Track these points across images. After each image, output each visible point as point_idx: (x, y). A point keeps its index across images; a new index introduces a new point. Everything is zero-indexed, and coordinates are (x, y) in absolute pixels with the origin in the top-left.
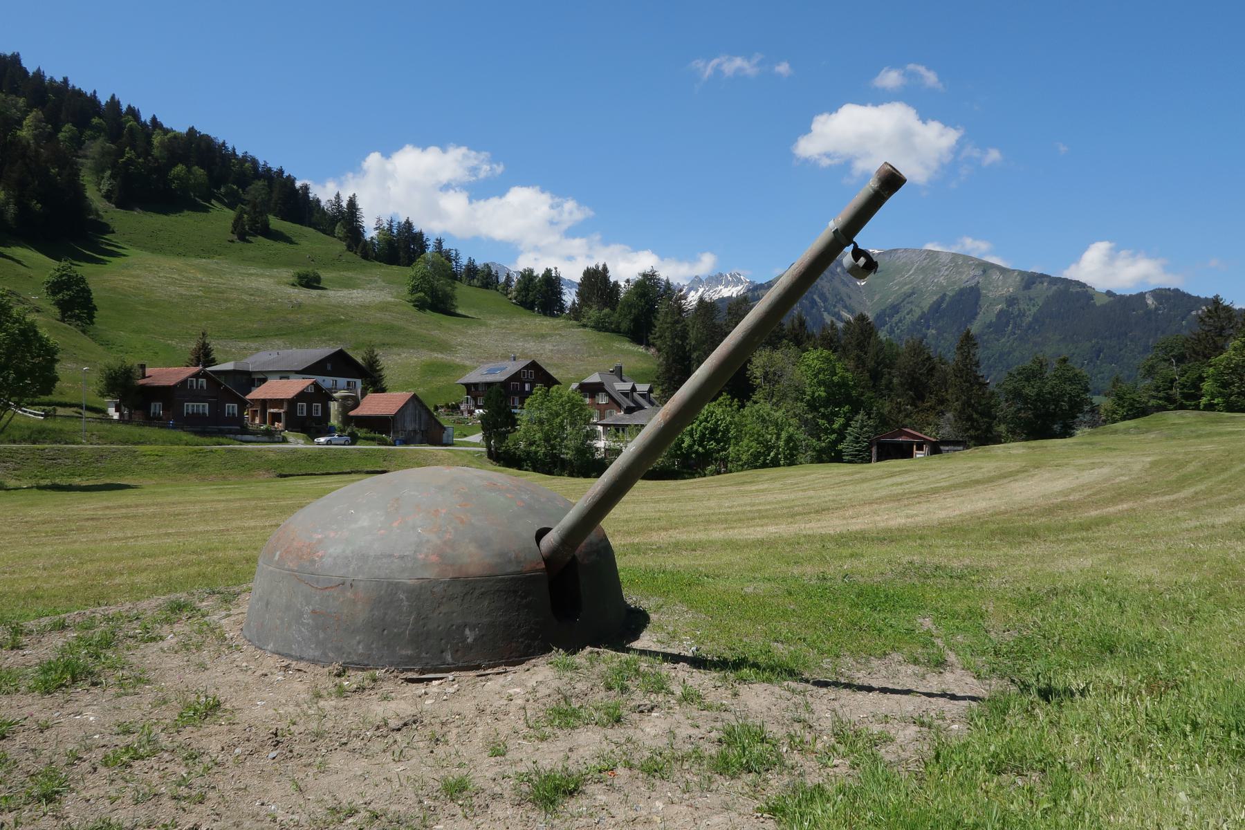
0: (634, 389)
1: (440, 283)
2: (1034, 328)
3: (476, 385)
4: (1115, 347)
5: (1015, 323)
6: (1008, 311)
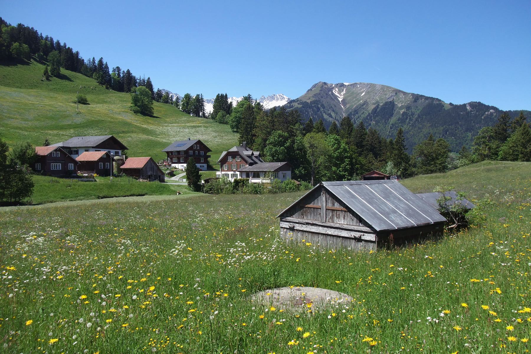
0: (253, 154)
1: (146, 100)
2: (418, 121)
3: (172, 152)
4: (453, 129)
5: (410, 118)
6: (407, 113)
